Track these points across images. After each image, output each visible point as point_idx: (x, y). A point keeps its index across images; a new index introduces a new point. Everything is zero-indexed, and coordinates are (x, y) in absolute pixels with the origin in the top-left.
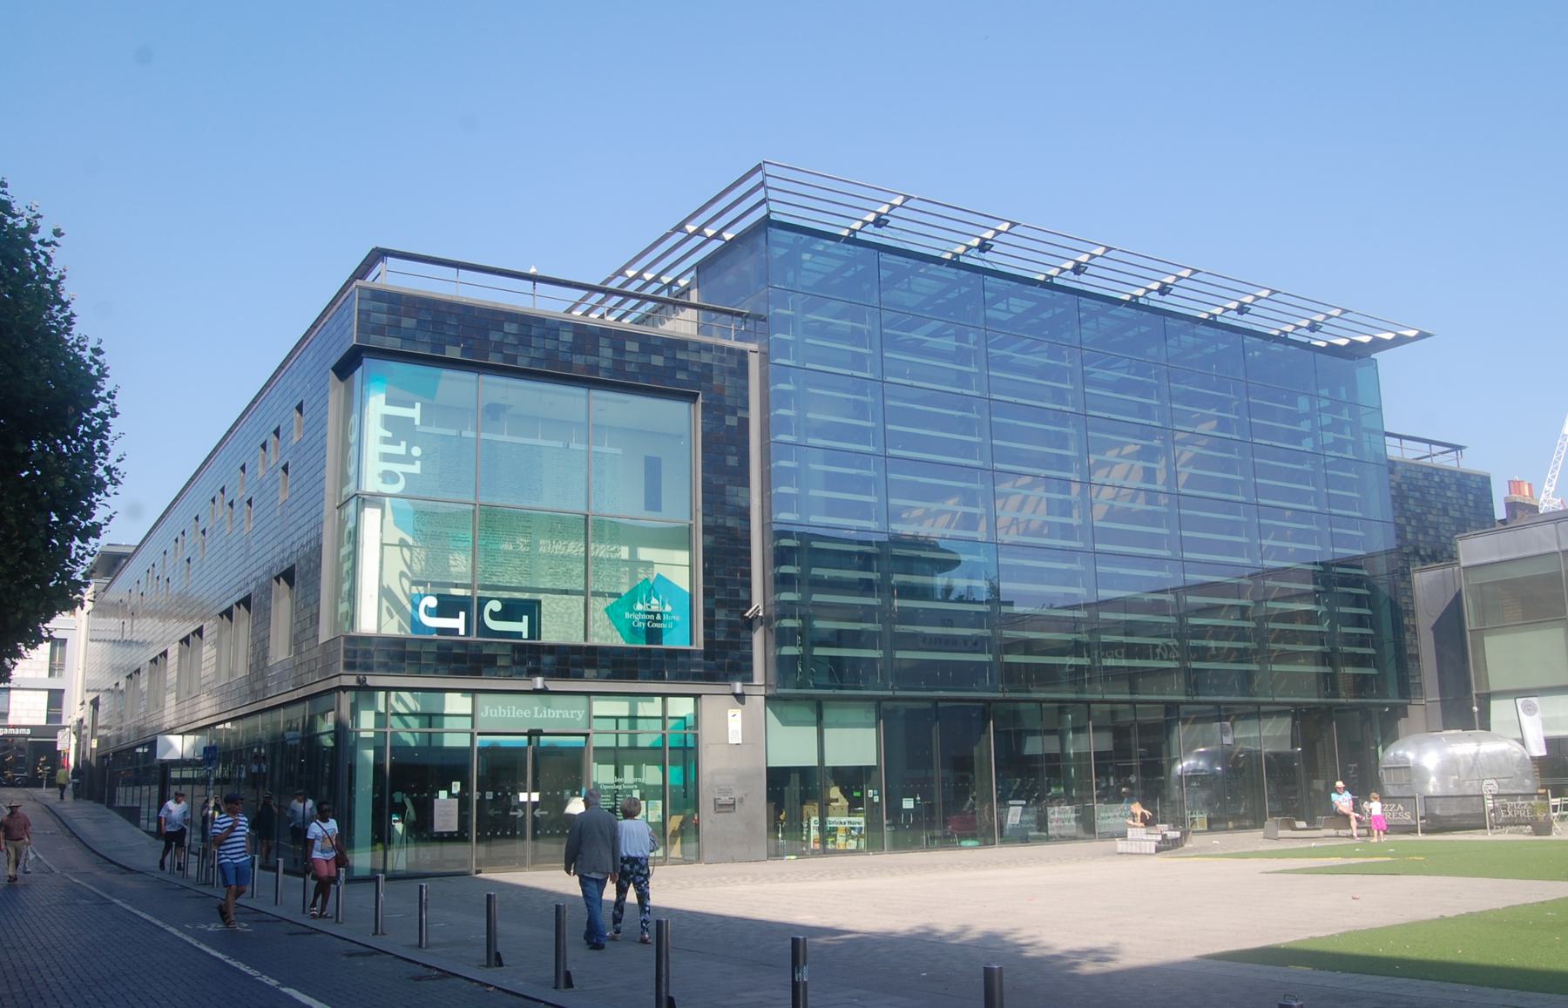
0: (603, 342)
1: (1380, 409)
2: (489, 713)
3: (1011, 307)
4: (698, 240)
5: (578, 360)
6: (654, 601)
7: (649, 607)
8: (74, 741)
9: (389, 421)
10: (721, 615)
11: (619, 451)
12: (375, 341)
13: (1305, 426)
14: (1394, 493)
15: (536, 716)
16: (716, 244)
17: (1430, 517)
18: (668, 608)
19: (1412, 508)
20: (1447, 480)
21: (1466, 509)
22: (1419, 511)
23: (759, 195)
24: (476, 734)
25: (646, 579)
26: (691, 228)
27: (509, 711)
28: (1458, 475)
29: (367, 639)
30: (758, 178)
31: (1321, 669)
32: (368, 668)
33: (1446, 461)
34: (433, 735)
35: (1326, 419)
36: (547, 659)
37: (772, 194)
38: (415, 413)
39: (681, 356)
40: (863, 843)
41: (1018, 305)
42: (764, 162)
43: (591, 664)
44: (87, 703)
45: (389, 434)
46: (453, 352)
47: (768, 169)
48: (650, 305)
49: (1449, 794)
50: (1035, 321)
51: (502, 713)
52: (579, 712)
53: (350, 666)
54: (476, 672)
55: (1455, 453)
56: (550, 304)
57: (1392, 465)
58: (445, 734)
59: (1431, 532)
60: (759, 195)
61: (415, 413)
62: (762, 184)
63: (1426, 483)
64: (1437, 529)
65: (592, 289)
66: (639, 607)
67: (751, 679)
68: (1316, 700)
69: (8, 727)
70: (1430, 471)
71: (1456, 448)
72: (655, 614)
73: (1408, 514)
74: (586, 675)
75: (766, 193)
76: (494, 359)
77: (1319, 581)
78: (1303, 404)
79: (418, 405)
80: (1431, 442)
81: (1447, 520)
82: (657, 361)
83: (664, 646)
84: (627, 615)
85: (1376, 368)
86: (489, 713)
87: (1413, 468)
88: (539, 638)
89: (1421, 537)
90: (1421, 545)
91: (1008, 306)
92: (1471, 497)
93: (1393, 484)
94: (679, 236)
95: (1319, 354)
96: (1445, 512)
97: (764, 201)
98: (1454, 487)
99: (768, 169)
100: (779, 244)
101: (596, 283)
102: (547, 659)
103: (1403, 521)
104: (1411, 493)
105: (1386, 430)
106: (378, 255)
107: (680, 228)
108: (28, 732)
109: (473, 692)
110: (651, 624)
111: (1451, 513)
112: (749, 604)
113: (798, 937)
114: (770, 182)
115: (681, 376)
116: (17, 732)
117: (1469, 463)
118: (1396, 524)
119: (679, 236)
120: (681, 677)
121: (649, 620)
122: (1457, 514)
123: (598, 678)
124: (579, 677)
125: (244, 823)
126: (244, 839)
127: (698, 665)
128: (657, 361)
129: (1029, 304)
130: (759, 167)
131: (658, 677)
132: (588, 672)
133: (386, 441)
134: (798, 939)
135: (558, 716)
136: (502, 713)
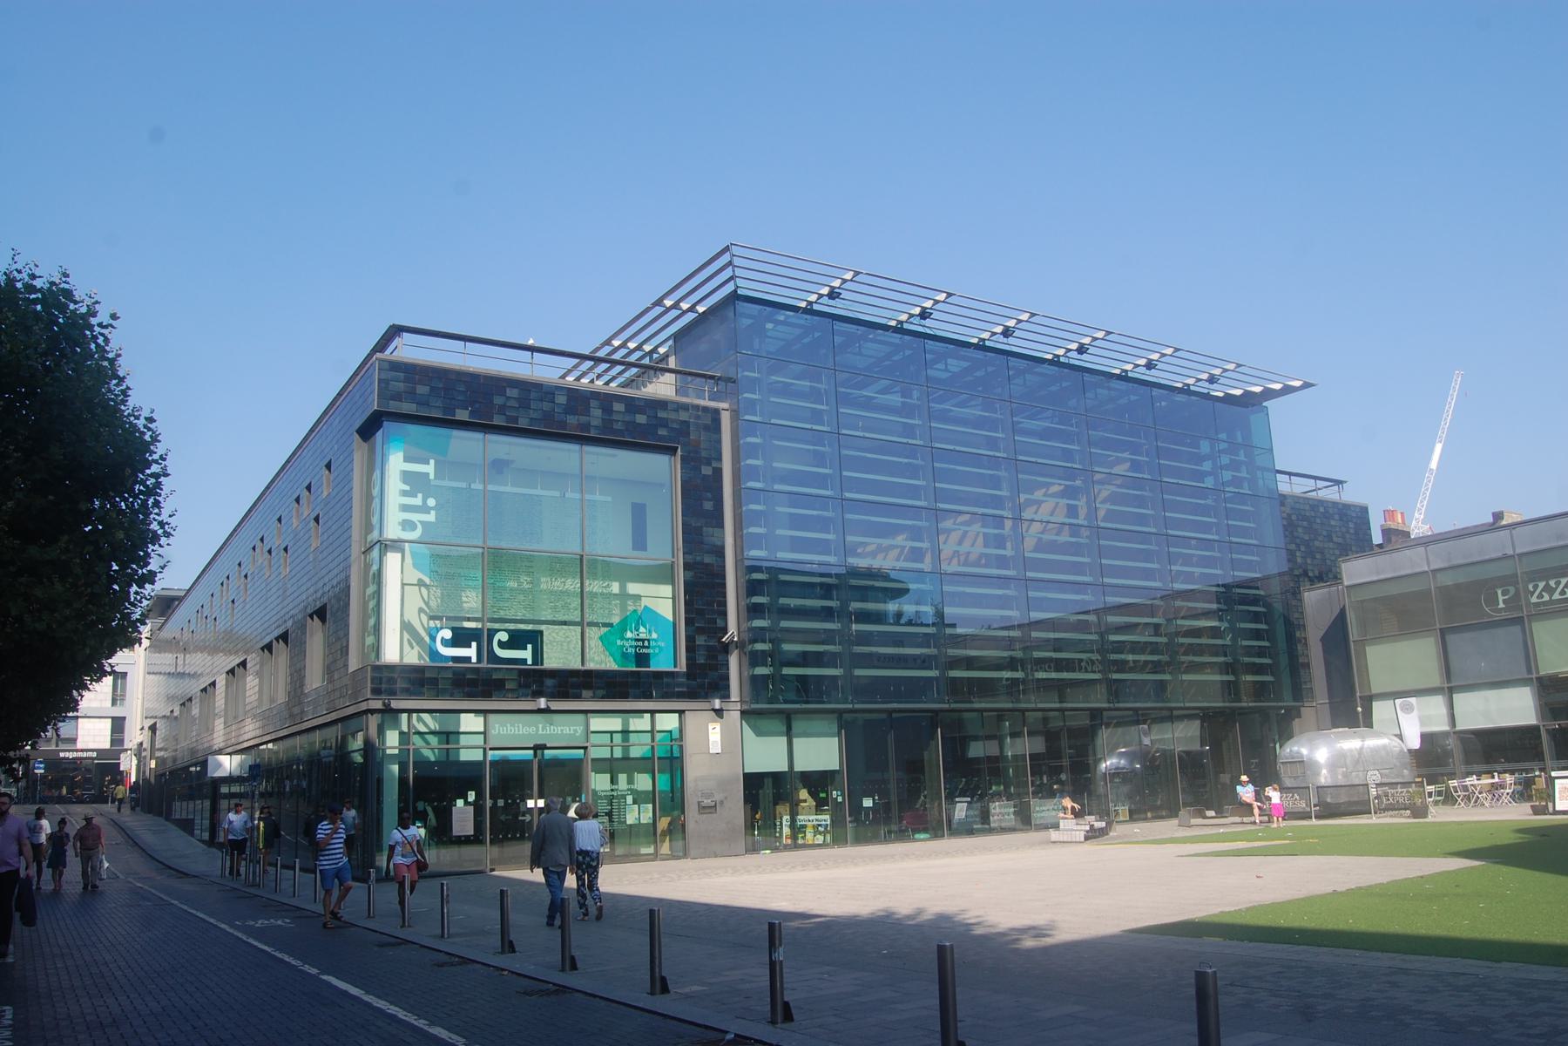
0: (593, 403)
1: (1272, 450)
2: (499, 730)
3: (949, 367)
4: (675, 313)
5: (572, 420)
8: (135, 762)
9: (407, 477)
11: (609, 499)
12: (394, 406)
13: (1207, 466)
15: (540, 732)
16: (691, 316)
17: (1317, 543)
18: (654, 636)
20: (1331, 511)
21: (1348, 536)
23: (728, 273)
26: (668, 303)
28: (1340, 506)
29: (391, 668)
30: (725, 258)
32: (392, 693)
33: (1330, 494)
35: (1225, 460)
36: (549, 682)
37: (738, 272)
38: (429, 468)
39: (661, 414)
41: (955, 365)
42: (731, 244)
43: (589, 686)
44: (146, 728)
45: (407, 488)
46: (462, 415)
47: (735, 250)
48: (634, 370)
50: (971, 378)
51: (511, 730)
53: (377, 692)
54: (486, 695)
56: (547, 371)
59: (1318, 556)
60: (728, 273)
61: (429, 468)
62: (730, 263)
65: (583, 357)
66: (629, 635)
67: (729, 697)
69: (77, 751)
70: (1316, 503)
71: (1338, 483)
72: (643, 640)
73: (1298, 541)
74: (583, 696)
75: (734, 271)
78: (1205, 447)
79: (432, 462)
80: (1316, 478)
81: (1331, 545)
84: (619, 642)
86: (499, 730)
88: (542, 664)
89: (1309, 561)
90: (1309, 567)
91: (946, 367)
92: (1351, 525)
93: (1285, 515)
94: (658, 310)
96: (1330, 539)
97: (731, 278)
98: (1337, 517)
99: (735, 250)
101: (587, 353)
103: (1293, 547)
105: (1277, 468)
106: (395, 331)
107: (659, 303)
108: (95, 755)
109: (485, 712)
111: (1335, 539)
112: (725, 631)
113: (774, 921)
114: (737, 261)
115: (662, 432)
116: (85, 755)
117: (1349, 495)
119: (658, 310)
120: (667, 696)
123: (594, 698)
124: (578, 697)
128: (641, 419)
129: (965, 364)
130: (727, 249)
131: (647, 696)
132: (585, 693)
133: (404, 493)
134: (1205, 973)
135: (559, 732)
136: (511, 730)
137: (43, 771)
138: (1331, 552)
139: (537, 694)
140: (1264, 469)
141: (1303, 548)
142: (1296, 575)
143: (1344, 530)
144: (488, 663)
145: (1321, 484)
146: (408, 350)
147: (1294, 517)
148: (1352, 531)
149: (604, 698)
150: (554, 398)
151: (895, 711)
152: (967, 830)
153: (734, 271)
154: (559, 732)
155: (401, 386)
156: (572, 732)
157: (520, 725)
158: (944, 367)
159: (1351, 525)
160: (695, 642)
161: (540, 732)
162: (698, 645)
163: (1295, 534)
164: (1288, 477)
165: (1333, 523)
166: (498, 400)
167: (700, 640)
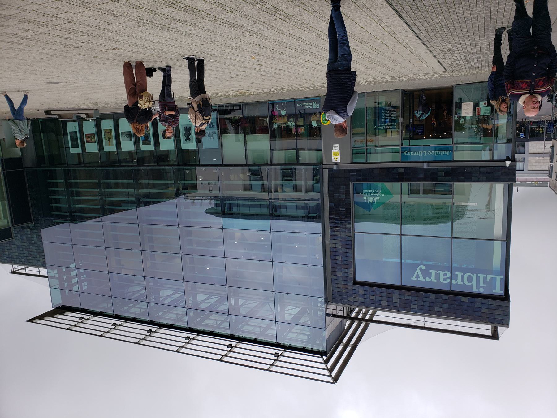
0: (397, 305)
1: (50, 288)
2: (447, 153)
6: (371, 201)
7: (373, 198)
10: (343, 196)
11: (385, 259)
12: (500, 303)
14: (42, 254)
15: (425, 152)
17: (26, 244)
19: (33, 248)
20: (18, 260)
21: (9, 248)
22: (31, 247)
24: (400, 145)
25: (74, 205)
27: (438, 153)
28: (13, 262)
30: (333, 374)
31: (55, 181)
33: (17, 267)
34: (409, 145)
36: (421, 175)
37: (323, 366)
40: (72, 127)
43: (401, 174)
46: (464, 299)
47: (330, 379)
49: (478, 81)
51: (418, 153)
52: (406, 154)
55: (14, 270)
57: (44, 265)
58: (505, 142)
59: (25, 238)
60: (329, 365)
63: (28, 258)
64: (22, 240)
68: (57, 169)
70: (26, 263)
71: (14, 272)
73: (36, 245)
74: (403, 169)
76: (446, 297)
77: (76, 217)
80: (26, 274)
81: (18, 244)
82: (373, 298)
83: (408, 182)
85: (52, 305)
86: (447, 153)
87: (34, 264)
89: (30, 236)
90: (29, 233)
92: (7, 253)
93: (43, 257)
95: (80, 307)
96: (18, 247)
100: (184, 322)
102: (421, 175)
103: (38, 242)
104: (35, 254)
105: (47, 279)
110: (373, 191)
111: (15, 246)
114: (327, 373)
115: (362, 292)
118: (42, 241)
121: (373, 193)
122: (13, 246)
123: (397, 169)
124: (406, 169)
125: (383, 119)
126: (392, 111)
127: (352, 176)
128: (373, 298)
130: (336, 379)
132: (402, 171)
135: (416, 152)
136: (418, 153)
137: (521, 133)
138: (17, 240)
139: (429, 169)
140: (54, 278)
141: (33, 242)
142: (36, 229)
143: (11, 251)
144: (302, 181)
145: (23, 271)
146: (486, 329)
147: (38, 256)
148: (6, 250)
149: (393, 169)
150: (417, 307)
151: (118, 166)
152: (280, 103)
153: (327, 367)
154: (416, 152)
155: (497, 312)
156: (409, 152)
157: (436, 155)
158: (142, 310)
159: (7, 253)
160: (345, 196)
161: (425, 152)
162: (343, 194)
163: (37, 248)
164: (27, 273)
165: (17, 254)
166: (445, 306)
167: (343, 196)
